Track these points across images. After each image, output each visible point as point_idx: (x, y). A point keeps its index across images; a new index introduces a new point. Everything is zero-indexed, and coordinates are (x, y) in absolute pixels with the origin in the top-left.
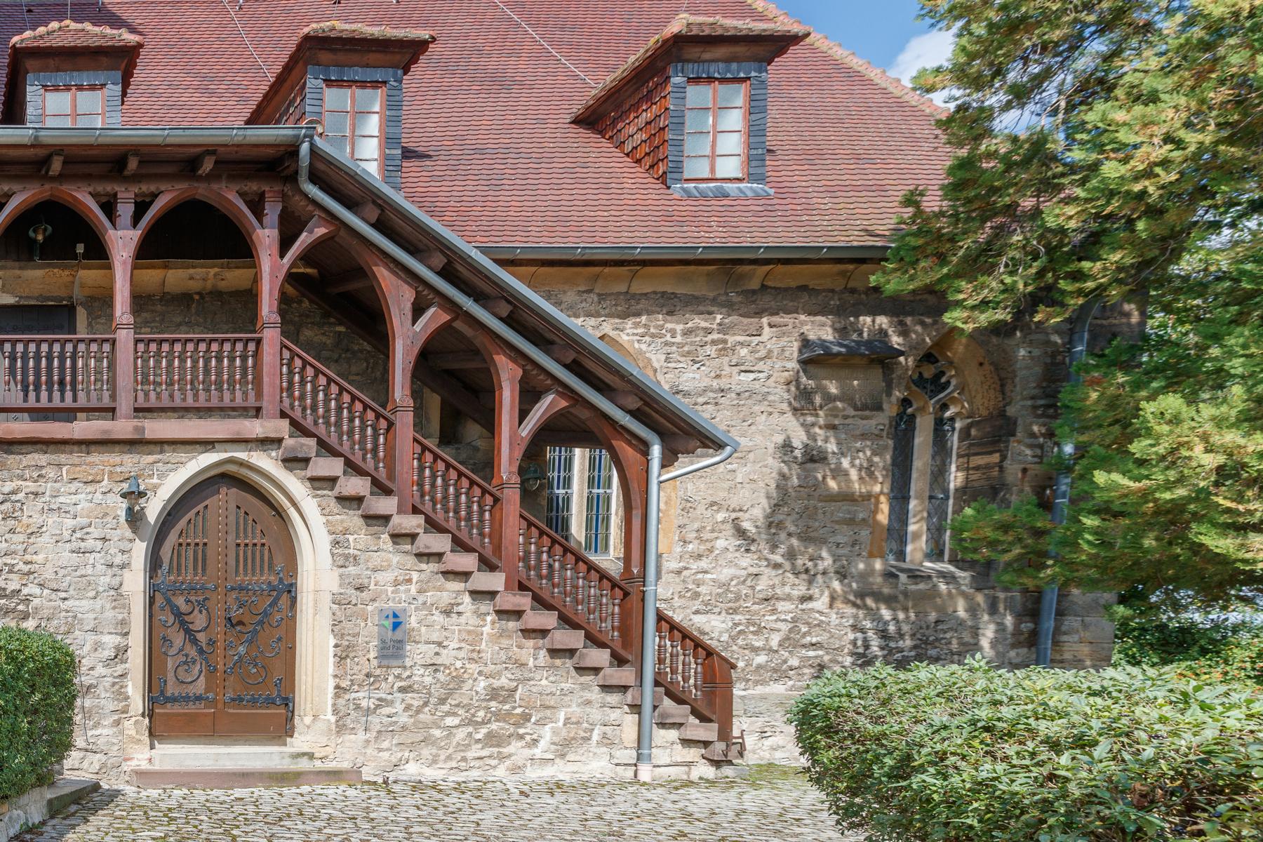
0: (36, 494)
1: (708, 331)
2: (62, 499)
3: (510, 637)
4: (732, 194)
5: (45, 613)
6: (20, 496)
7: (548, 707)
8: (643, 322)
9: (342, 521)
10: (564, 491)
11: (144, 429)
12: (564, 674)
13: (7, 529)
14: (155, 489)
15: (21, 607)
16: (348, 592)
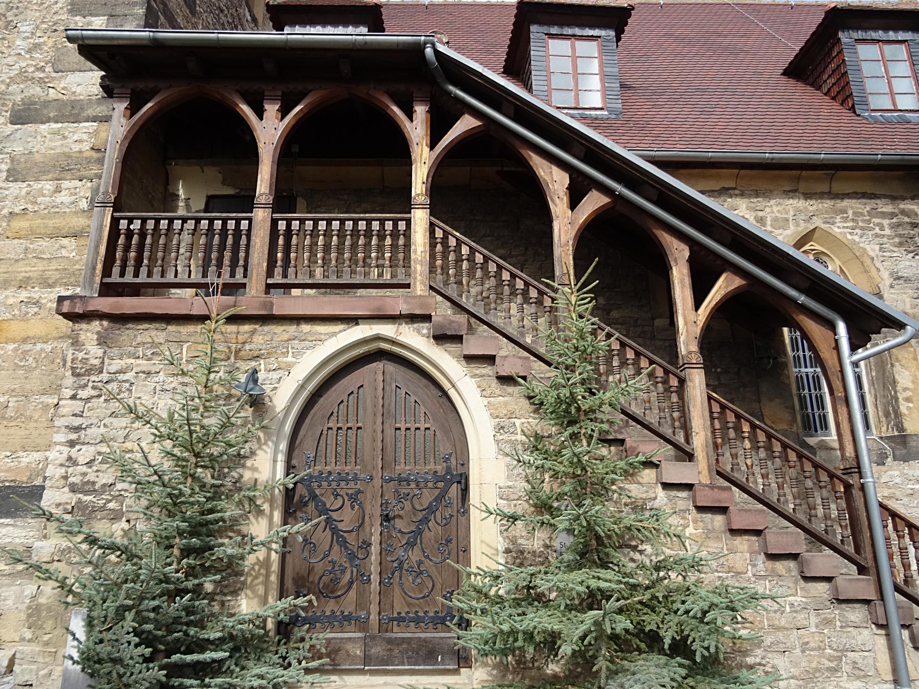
3: (719, 539)
4: (913, 121)
6: (129, 376)
7: (779, 629)
8: (851, 217)
9: (506, 404)
10: (812, 370)
11: (272, 304)
12: (791, 585)
13: (109, 412)
15: (111, 505)
16: (517, 484)
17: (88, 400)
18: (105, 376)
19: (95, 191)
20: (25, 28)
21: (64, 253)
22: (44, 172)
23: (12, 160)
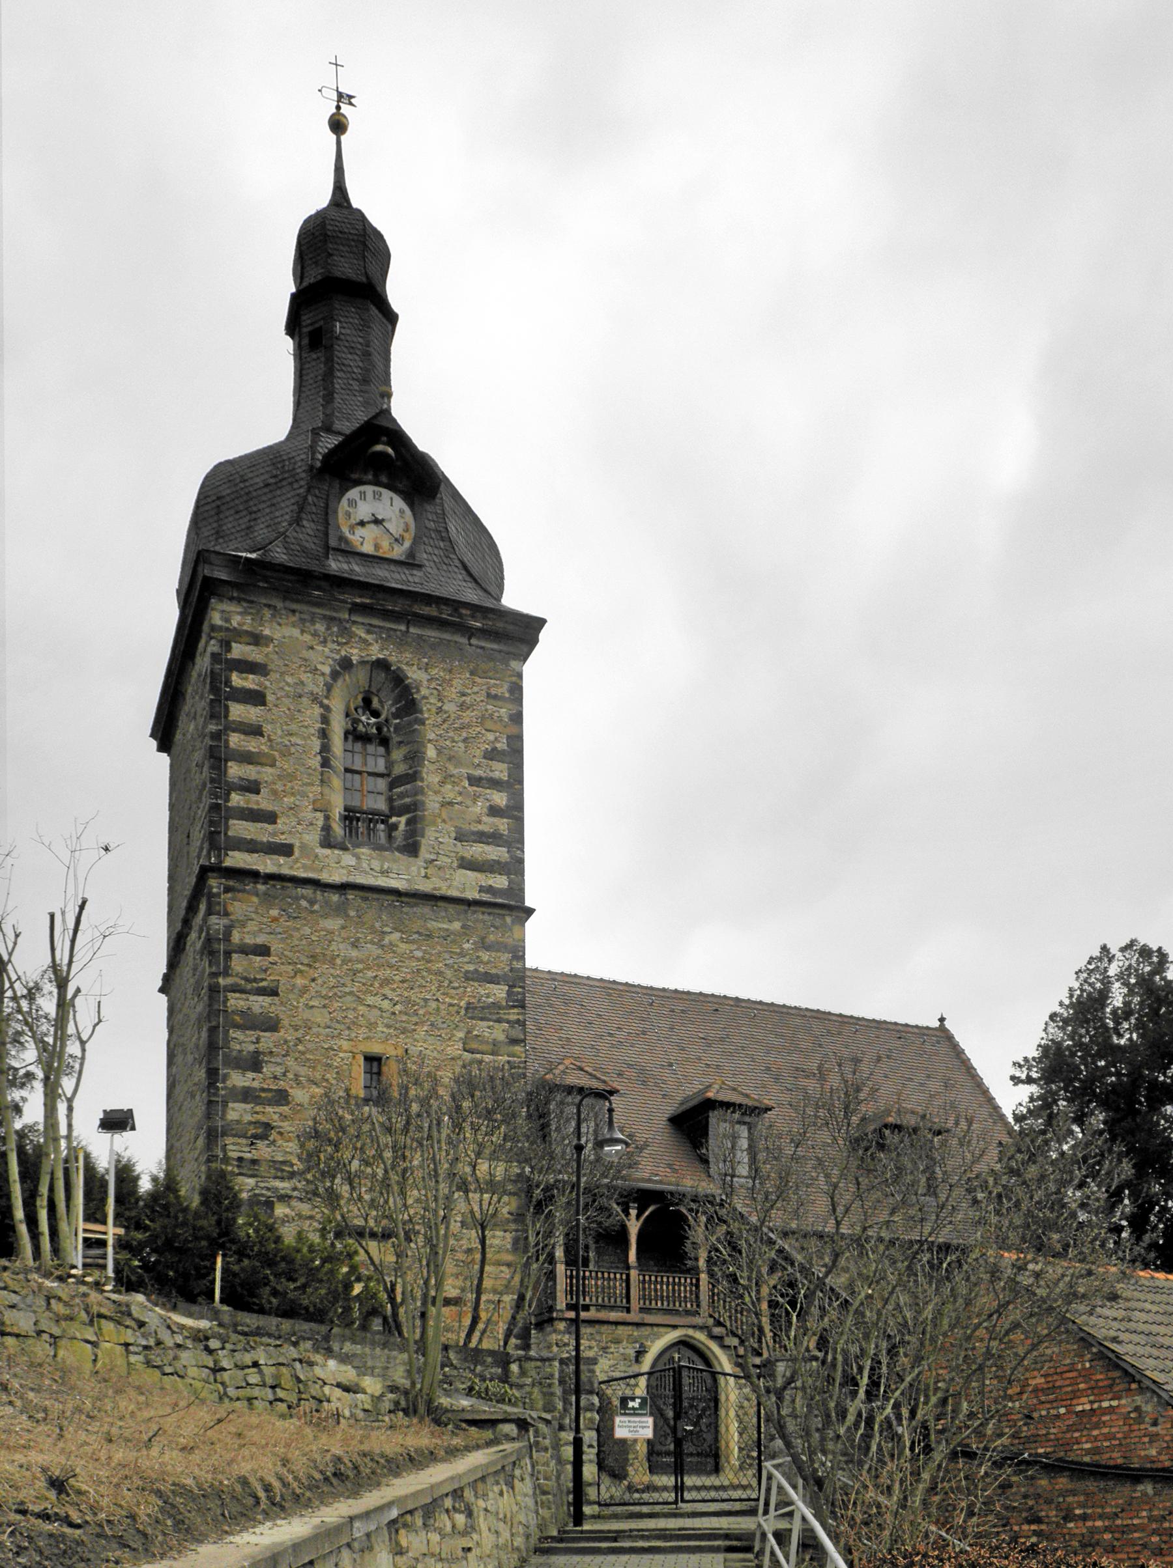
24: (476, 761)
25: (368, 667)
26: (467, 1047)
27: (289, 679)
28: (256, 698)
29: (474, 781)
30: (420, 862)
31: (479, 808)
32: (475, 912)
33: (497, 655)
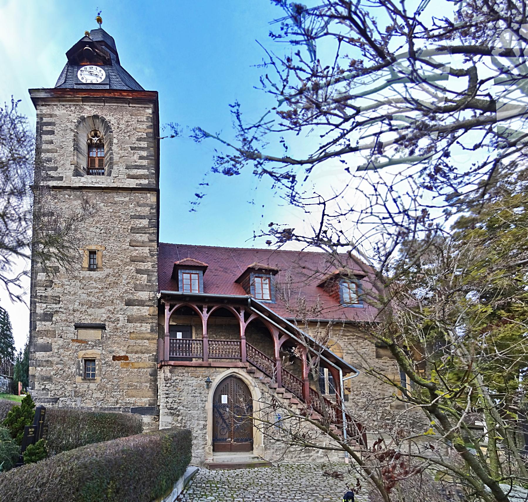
0: (182, 380)
1: (353, 339)
2: (189, 382)
5: (184, 414)
6: (178, 381)
14: (214, 379)
15: (177, 413)
17: (169, 387)
18: (172, 381)
19: (152, 327)
20: (125, 277)
21: (146, 344)
22: (137, 321)
23: (128, 317)
24: (134, 142)
25: (91, 118)
26: (131, 244)
27: (62, 125)
28: (52, 133)
29: (132, 148)
30: (111, 178)
31: (136, 157)
32: (134, 193)
33: (141, 109)
